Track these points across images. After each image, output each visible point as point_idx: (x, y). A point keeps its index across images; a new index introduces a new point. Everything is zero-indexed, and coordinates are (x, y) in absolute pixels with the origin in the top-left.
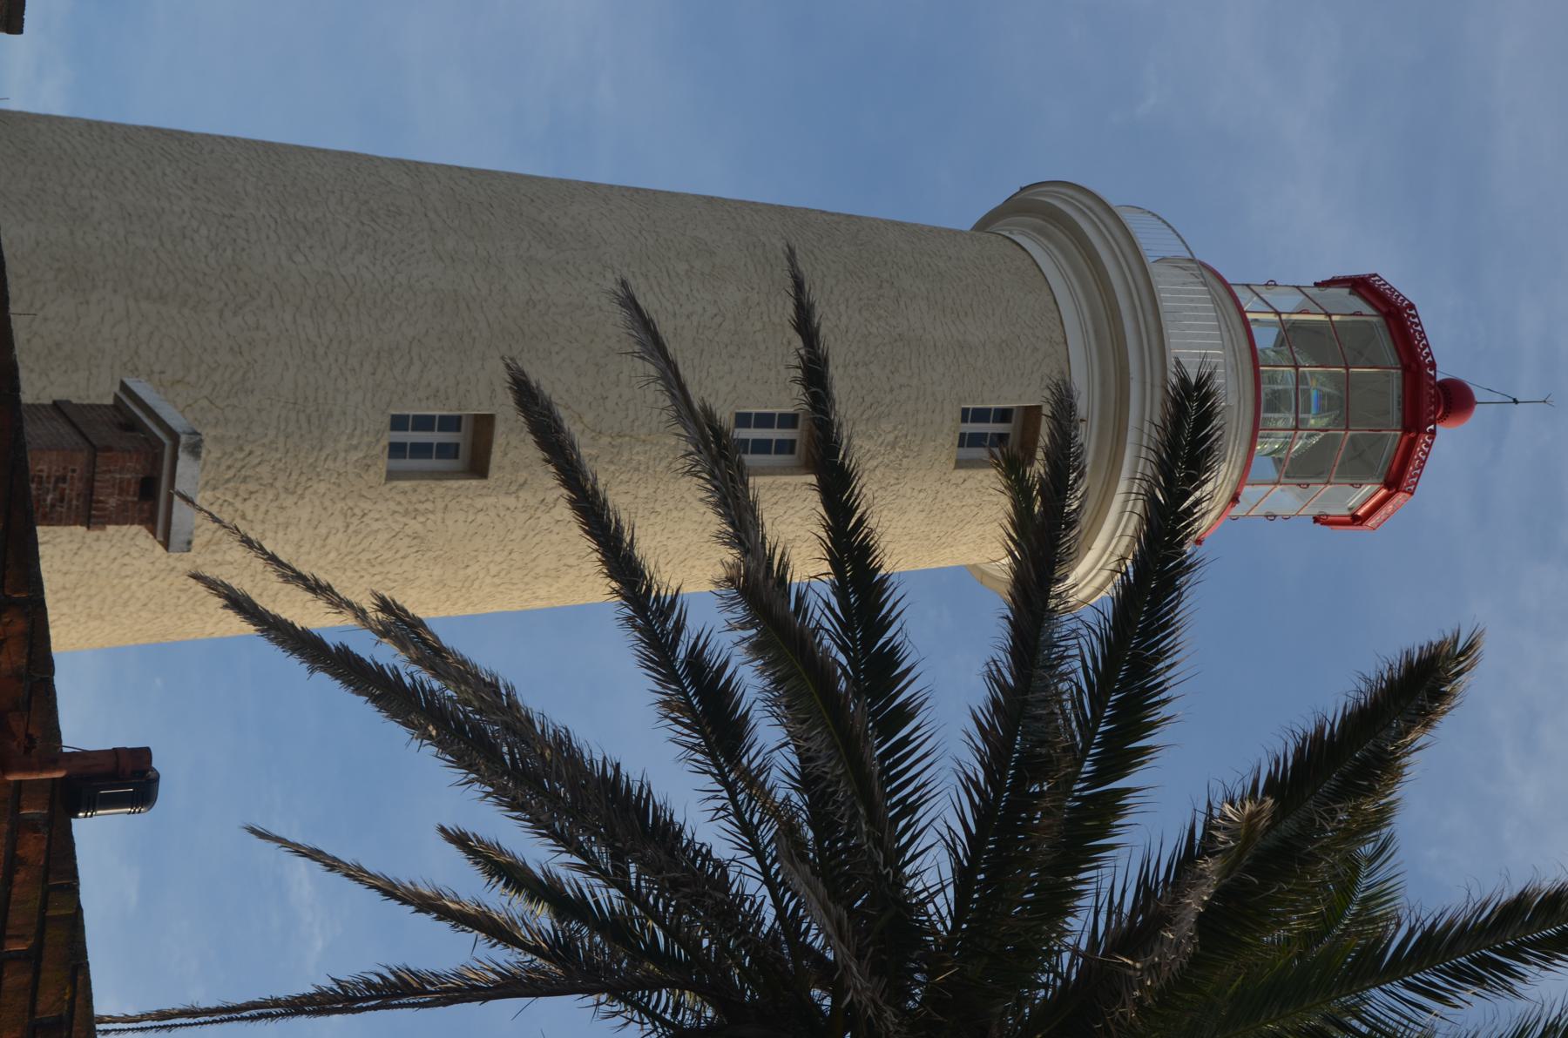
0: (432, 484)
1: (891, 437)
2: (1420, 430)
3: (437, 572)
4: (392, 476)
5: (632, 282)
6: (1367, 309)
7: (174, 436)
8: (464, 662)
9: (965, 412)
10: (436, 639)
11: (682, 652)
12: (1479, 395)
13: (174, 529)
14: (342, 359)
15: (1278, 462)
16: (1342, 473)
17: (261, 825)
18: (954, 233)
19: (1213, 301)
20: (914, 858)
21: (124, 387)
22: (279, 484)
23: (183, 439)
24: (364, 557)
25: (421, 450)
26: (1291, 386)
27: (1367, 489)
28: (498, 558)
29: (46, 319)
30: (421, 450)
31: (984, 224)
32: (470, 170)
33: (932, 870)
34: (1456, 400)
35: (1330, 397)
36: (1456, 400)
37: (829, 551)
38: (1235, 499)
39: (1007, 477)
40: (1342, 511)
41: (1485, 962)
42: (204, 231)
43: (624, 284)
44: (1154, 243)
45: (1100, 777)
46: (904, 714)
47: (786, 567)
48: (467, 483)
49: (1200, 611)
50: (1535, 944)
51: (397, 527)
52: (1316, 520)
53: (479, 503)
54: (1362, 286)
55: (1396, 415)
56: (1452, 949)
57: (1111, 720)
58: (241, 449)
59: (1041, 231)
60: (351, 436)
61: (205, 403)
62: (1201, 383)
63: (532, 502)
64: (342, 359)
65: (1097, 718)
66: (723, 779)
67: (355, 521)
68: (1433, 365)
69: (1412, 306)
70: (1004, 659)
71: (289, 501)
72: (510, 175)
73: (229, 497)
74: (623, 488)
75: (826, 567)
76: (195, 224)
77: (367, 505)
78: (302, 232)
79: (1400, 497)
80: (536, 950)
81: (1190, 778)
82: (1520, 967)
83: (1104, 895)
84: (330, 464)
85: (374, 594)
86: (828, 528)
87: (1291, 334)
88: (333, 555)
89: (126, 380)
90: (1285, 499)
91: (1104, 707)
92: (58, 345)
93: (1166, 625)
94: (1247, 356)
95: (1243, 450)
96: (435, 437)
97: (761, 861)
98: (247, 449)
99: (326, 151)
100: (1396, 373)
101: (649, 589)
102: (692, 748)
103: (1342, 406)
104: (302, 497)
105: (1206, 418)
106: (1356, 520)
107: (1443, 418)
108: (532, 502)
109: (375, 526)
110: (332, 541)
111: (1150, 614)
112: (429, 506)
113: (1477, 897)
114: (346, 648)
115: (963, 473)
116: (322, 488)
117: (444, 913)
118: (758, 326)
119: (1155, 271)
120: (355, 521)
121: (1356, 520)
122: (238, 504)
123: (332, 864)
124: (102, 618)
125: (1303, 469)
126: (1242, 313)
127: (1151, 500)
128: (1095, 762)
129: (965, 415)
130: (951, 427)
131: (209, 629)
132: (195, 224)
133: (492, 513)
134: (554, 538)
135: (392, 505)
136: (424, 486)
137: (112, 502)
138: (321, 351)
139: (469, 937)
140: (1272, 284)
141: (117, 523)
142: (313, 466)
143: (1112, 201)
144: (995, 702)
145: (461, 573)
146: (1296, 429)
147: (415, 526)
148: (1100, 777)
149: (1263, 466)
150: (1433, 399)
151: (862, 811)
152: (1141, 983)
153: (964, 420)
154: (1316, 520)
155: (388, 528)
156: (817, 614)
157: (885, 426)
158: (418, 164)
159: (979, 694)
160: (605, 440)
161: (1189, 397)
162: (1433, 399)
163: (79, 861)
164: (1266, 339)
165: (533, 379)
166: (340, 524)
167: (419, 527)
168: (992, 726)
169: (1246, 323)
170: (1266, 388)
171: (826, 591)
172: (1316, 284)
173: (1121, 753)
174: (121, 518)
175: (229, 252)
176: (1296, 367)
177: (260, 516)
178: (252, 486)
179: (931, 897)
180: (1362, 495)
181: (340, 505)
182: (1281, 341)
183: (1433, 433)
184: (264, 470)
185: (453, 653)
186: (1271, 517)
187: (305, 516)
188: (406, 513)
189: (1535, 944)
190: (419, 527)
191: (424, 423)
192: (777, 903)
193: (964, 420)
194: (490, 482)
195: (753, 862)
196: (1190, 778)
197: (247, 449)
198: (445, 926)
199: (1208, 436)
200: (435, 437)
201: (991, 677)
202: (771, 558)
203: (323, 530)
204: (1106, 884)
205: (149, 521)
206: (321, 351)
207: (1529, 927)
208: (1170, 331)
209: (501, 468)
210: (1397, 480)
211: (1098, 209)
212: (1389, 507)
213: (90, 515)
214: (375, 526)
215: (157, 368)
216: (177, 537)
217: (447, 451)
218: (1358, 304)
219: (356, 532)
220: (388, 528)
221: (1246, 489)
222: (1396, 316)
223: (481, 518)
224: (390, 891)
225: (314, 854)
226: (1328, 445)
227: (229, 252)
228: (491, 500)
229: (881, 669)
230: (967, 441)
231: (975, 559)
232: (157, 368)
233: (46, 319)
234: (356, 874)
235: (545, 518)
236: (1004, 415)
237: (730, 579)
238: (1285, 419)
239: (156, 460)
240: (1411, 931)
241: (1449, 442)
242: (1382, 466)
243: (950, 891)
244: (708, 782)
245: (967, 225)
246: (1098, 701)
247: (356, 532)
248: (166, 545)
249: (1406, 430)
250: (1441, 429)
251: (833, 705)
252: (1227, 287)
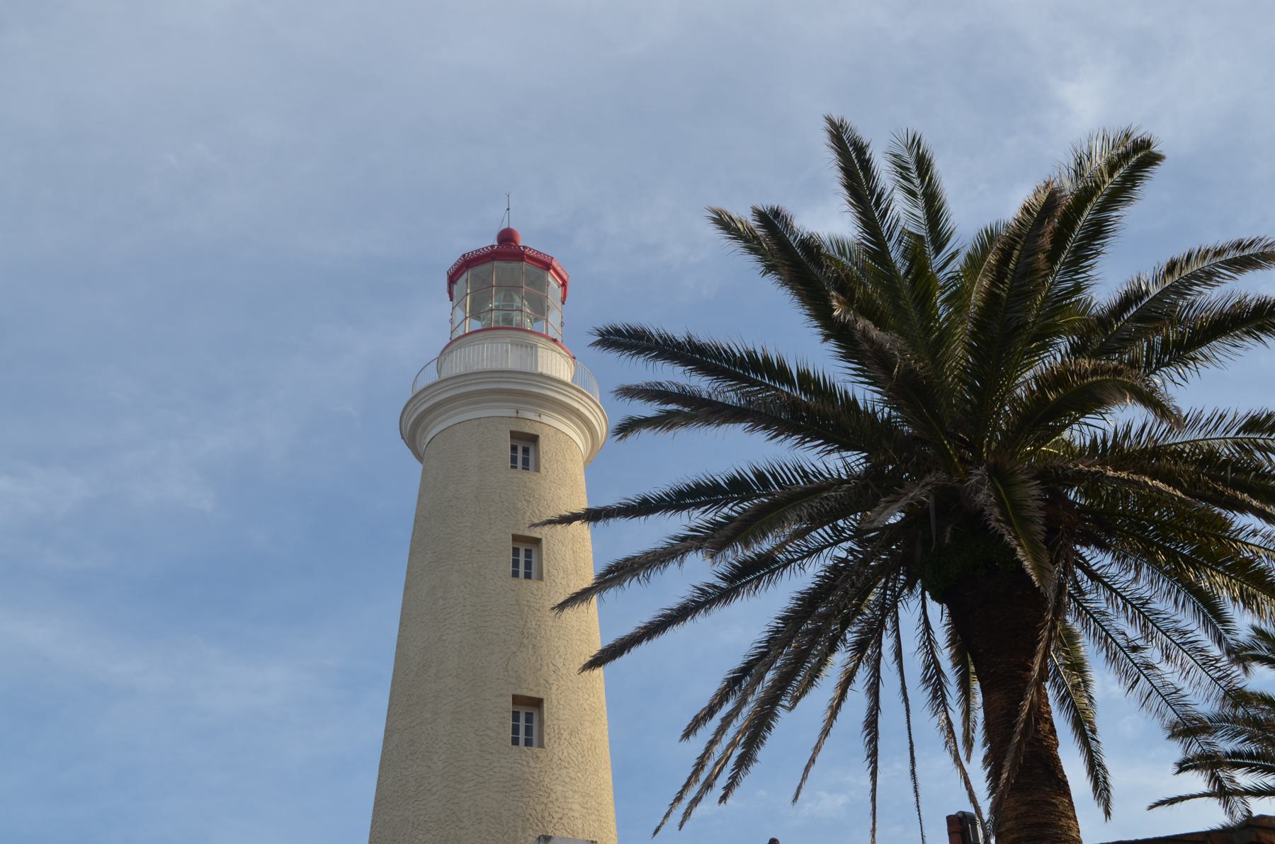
2: (523, 253)
3: (587, 724)
4: (541, 745)
6: (464, 277)
12: (505, 226)
15: (536, 320)
17: (791, 797)
18: (424, 471)
25: (529, 731)
27: (550, 279)
30: (529, 731)
31: (420, 457)
34: (507, 237)
36: (507, 237)
38: (555, 341)
40: (560, 291)
41: (878, 204)
44: (431, 376)
45: (790, 382)
50: (868, 183)
53: (555, 703)
54: (453, 279)
55: (515, 265)
56: (873, 219)
59: (424, 430)
62: (602, 334)
65: (761, 384)
66: (785, 566)
71: (553, 796)
75: (685, 513)
77: (556, 758)
80: (860, 659)
81: (795, 339)
82: (878, 190)
86: (666, 511)
87: (475, 314)
90: (554, 317)
91: (756, 381)
93: (717, 349)
94: (487, 333)
95: (531, 336)
97: (825, 547)
100: (496, 263)
102: (769, 581)
103: (510, 288)
105: (618, 332)
106: (564, 285)
108: (554, 676)
110: (572, 775)
111: (711, 357)
115: (542, 469)
116: (547, 779)
119: (444, 376)
121: (564, 285)
125: (540, 310)
127: (656, 357)
130: (519, 474)
136: (547, 730)
139: (850, 693)
142: (537, 784)
143: (410, 396)
144: (764, 428)
147: (566, 735)
148: (790, 382)
150: (508, 246)
152: (910, 359)
159: (760, 437)
160: (525, 641)
162: (508, 246)
163: (1163, 835)
164: (477, 325)
165: (589, 659)
166: (565, 771)
169: (470, 333)
170: (501, 325)
171: (696, 513)
173: (781, 373)
178: (546, 814)
182: (478, 318)
184: (539, 808)
185: (712, 700)
186: (562, 324)
187: (560, 788)
189: (868, 183)
191: (515, 730)
192: (846, 539)
194: (545, 697)
195: (825, 551)
196: (795, 339)
203: (568, 780)
207: (860, 184)
212: (558, 269)
217: (529, 718)
218: (462, 281)
222: (468, 263)
224: (825, 732)
225: (807, 769)
226: (529, 297)
229: (737, 487)
234: (817, 748)
236: (514, 449)
237: (712, 557)
238: (517, 317)
242: (539, 271)
243: (844, 454)
245: (420, 466)
246: (753, 383)
249: (523, 260)
251: (761, 511)
252: (452, 342)
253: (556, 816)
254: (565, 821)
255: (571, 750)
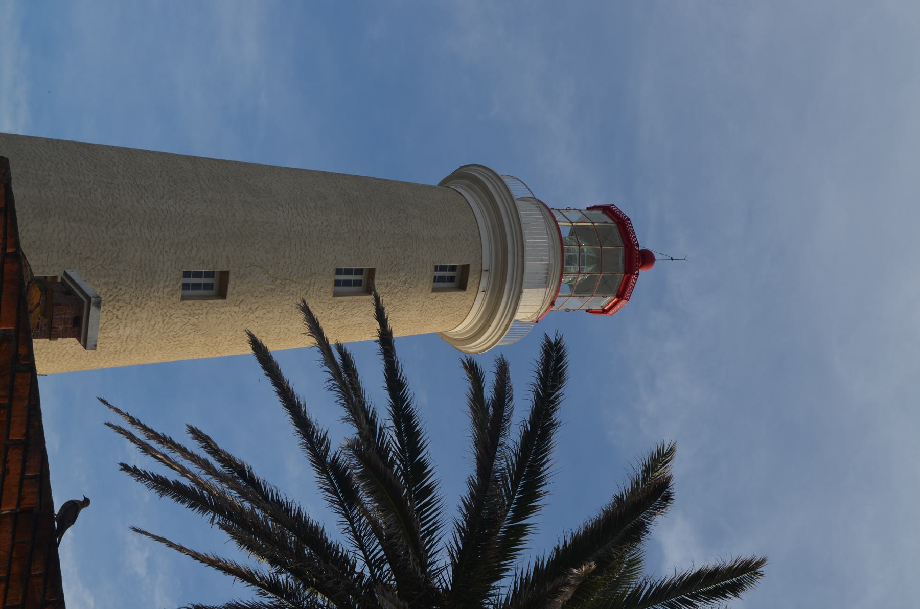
0: (202, 302)
1: (404, 279)
2: (632, 273)
3: (203, 339)
4: (184, 298)
5: (307, 302)
7: (88, 298)
8: (229, 456)
9: (436, 267)
10: (215, 445)
11: (329, 460)
12: (657, 256)
13: (89, 340)
14: (161, 247)
16: (598, 292)
19: (544, 218)
20: (432, 555)
21: (65, 274)
22: (133, 303)
23: (93, 300)
24: (171, 334)
25: (197, 286)
26: (577, 254)
27: (609, 298)
28: (231, 333)
29: (28, 231)
30: (197, 286)
31: (443, 183)
32: (218, 160)
33: (442, 559)
34: (647, 258)
35: (592, 258)
36: (647, 258)
37: (393, 416)
38: (552, 304)
39: (470, 373)
42: (99, 190)
43: (304, 302)
44: (518, 191)
45: (515, 518)
46: (428, 490)
47: (375, 415)
48: (217, 301)
49: (561, 445)
51: (186, 321)
52: (587, 311)
53: (222, 310)
54: (607, 210)
55: (621, 266)
56: (669, 596)
57: (520, 493)
58: (116, 287)
60: (166, 281)
61: (100, 267)
62: (557, 343)
63: (246, 309)
64: (161, 247)
65: (514, 491)
66: (347, 516)
67: (167, 318)
68: (638, 245)
69: (629, 219)
70: (475, 474)
71: (138, 310)
72: (236, 162)
73: (111, 309)
74: (286, 302)
76: (95, 187)
78: (143, 191)
79: (623, 302)
83: (519, 574)
84: (156, 294)
85: (188, 426)
86: (392, 406)
88: (157, 333)
89: (68, 272)
90: (575, 303)
92: (34, 242)
93: (546, 450)
94: (558, 241)
95: (556, 282)
96: (203, 280)
97: (365, 553)
98: (119, 287)
99: (154, 152)
101: (313, 432)
102: (333, 502)
103: (599, 262)
104: (143, 308)
105: (560, 358)
106: (604, 311)
107: (642, 266)
108: (246, 309)
109: (176, 320)
110: (157, 327)
112: (200, 311)
113: (680, 573)
114: (178, 482)
115: (435, 294)
116: (152, 304)
117: (220, 568)
118: (346, 230)
120: (167, 318)
121: (604, 311)
122: (115, 312)
123: (170, 545)
124: (53, 362)
126: (556, 222)
127: (538, 395)
128: (513, 511)
129: (436, 268)
130: (430, 273)
131: (101, 365)
132: (95, 187)
133: (228, 314)
134: (255, 324)
135: (183, 311)
136: (198, 303)
137: (61, 328)
138: (152, 244)
140: (568, 209)
141: (63, 337)
142: (148, 295)
143: (499, 173)
144: (472, 494)
145: (214, 340)
146: (579, 273)
147: (194, 320)
148: (515, 518)
149: (565, 287)
151: (410, 551)
153: (436, 270)
154: (587, 311)
155: (182, 321)
156: (389, 437)
157: (402, 274)
158: (195, 157)
159: (465, 491)
160: (278, 282)
161: (552, 349)
164: (565, 233)
166: (160, 319)
167: (195, 321)
168: (471, 505)
169: (557, 226)
170: (566, 254)
172: (588, 209)
173: (525, 508)
174: (65, 335)
175: (111, 200)
176: (579, 246)
177: (124, 317)
178: (121, 304)
179: (440, 572)
180: (606, 301)
181: (160, 311)
182: (572, 234)
183: (637, 274)
184: (127, 297)
185: (223, 452)
186: (568, 310)
187: (145, 316)
188: (190, 314)
189: (703, 593)
190: (195, 321)
191: (198, 274)
192: (372, 572)
193: (436, 270)
194: (227, 300)
195: (361, 552)
197: (119, 287)
198: (221, 573)
199: (562, 367)
200: (203, 280)
201: (470, 484)
202: (368, 412)
203: (153, 323)
204: (520, 566)
205: (78, 337)
206: (152, 244)
207: (702, 586)
208: (526, 232)
209: (232, 294)
210: (622, 294)
211: (494, 178)
212: (619, 306)
213: (51, 334)
214: (176, 320)
215: (78, 252)
216: (89, 344)
217: (208, 286)
218: (606, 218)
219: (167, 323)
220: (182, 321)
221: (558, 299)
222: (622, 223)
223: (223, 316)
224: (196, 556)
227: (111, 200)
228: (228, 308)
229: (417, 470)
230: (437, 279)
231: (440, 330)
232: (78, 252)
233: (28, 231)
234: (181, 549)
235: (252, 316)
236: (453, 268)
238: (573, 269)
239: (81, 309)
240: (651, 587)
241: (644, 275)
242: (616, 289)
244: (341, 518)
245: (435, 183)
246: (515, 484)
247: (167, 323)
248: (85, 347)
249: (626, 273)
250: (641, 271)
253: (119, 313)
254: (115, 321)
255: (179, 325)
